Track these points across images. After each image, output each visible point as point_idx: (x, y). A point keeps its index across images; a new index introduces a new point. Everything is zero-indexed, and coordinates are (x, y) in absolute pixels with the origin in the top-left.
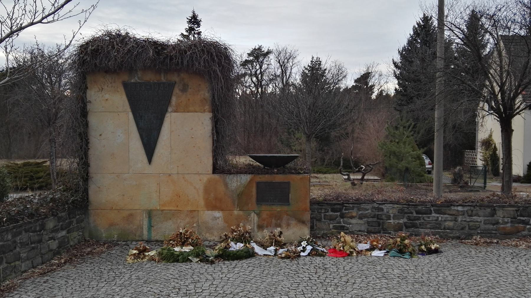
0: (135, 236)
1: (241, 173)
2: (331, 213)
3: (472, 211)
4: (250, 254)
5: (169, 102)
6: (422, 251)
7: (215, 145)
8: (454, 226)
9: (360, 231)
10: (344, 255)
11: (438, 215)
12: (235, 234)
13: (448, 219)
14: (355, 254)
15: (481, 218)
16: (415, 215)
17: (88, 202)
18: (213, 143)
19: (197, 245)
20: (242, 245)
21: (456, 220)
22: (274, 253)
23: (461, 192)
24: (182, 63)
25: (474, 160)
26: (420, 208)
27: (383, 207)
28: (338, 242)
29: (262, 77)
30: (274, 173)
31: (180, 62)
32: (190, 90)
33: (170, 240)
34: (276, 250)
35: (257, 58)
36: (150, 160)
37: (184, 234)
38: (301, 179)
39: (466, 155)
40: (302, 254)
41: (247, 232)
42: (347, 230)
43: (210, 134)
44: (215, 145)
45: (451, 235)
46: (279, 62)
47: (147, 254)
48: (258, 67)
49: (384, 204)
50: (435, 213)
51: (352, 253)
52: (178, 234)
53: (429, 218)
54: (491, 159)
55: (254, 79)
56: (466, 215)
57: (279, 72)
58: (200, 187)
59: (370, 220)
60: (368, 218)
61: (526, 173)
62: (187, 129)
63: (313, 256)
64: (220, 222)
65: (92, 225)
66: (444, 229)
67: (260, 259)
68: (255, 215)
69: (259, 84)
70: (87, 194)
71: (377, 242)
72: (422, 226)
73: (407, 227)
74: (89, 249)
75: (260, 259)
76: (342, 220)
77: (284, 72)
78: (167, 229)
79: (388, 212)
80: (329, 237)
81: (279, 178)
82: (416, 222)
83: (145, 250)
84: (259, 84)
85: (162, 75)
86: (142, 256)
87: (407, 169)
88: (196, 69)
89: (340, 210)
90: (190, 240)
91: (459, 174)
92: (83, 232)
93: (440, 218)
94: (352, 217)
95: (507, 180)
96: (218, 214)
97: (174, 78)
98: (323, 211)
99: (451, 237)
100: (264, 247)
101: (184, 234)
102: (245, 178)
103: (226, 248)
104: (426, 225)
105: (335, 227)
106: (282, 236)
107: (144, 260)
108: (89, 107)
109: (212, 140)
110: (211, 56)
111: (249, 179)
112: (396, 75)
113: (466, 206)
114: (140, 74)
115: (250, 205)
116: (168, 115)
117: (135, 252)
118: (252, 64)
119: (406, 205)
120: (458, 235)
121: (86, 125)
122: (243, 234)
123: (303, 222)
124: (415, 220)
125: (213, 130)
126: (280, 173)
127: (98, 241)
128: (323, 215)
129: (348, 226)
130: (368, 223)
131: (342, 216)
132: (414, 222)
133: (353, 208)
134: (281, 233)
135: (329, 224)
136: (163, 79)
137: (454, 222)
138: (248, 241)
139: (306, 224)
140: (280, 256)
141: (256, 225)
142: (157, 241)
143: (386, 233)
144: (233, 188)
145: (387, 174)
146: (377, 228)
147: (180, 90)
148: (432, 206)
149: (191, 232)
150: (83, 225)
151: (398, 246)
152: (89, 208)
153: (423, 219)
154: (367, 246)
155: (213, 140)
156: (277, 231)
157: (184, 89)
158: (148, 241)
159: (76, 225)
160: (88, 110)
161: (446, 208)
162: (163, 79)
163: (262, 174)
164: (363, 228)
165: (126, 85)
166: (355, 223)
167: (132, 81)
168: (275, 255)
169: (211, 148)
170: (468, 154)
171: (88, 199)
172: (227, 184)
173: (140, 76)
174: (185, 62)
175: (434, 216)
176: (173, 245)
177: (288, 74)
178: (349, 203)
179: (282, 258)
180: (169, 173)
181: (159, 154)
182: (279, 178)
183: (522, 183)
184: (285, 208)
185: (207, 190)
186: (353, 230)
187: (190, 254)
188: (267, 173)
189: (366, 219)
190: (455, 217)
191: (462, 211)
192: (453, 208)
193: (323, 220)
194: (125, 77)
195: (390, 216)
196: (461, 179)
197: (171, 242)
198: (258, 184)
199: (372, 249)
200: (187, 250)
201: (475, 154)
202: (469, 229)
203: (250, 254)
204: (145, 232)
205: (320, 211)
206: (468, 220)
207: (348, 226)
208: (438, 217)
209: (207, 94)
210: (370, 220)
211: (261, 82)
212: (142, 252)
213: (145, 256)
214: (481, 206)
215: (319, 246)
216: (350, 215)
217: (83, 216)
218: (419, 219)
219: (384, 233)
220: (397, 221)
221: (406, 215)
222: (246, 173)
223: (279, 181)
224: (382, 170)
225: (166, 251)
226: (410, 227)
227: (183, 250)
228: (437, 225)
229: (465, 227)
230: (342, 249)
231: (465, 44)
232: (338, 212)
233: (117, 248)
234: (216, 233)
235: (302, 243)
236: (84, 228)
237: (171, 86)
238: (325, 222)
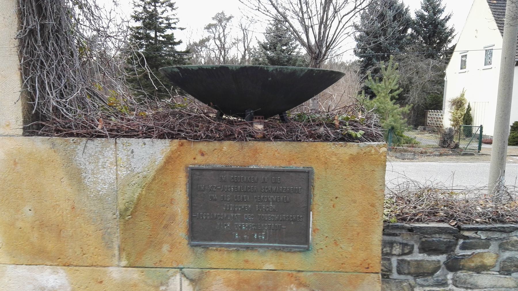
1: (131, 133)
23: (453, 155)
25: (440, 119)
29: (225, 40)
30: (252, 136)
35: (220, 21)
38: (354, 159)
39: (428, 115)
48: (221, 30)
54: (464, 119)
55: (218, 42)
68: (186, 283)
69: (222, 48)
76: (450, 276)
77: (245, 36)
81: (273, 155)
84: (222, 48)
89: (448, 248)
91: (449, 134)
94: (480, 269)
102: (149, 153)
111: (160, 159)
112: (355, 37)
115: (166, 248)
118: (216, 28)
126: (277, 138)
133: (486, 245)
144: (103, 188)
163: (209, 138)
172: (79, 172)
178: (476, 230)
184: (293, 261)
188: (229, 137)
196: (451, 141)
198: (195, 175)
201: (440, 114)
211: (224, 45)
216: (476, 262)
222: (148, 134)
223: (271, 167)
232: (442, 253)
238: (401, 282)
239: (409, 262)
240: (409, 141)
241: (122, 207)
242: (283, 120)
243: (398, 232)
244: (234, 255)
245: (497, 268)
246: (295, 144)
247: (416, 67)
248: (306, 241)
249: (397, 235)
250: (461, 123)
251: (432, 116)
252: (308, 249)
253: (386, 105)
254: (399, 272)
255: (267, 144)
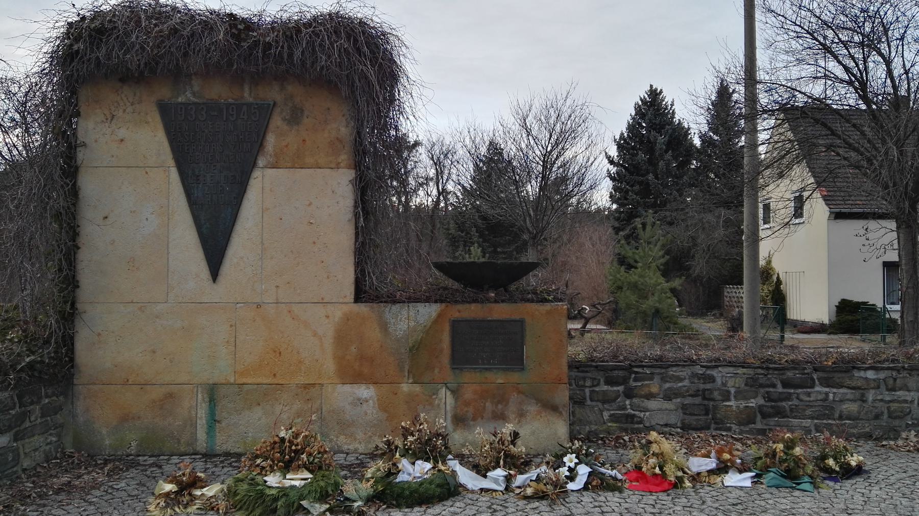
0: (179, 442)
1: (417, 300)
2: (606, 388)
3: (895, 380)
4: (449, 490)
5: (260, 146)
6: (828, 470)
7: (361, 239)
8: (859, 413)
9: (666, 425)
10: (666, 485)
11: (827, 390)
12: (410, 438)
13: (849, 397)
14: (688, 484)
15: (912, 394)
16: (780, 389)
17: (72, 367)
18: (357, 234)
19: (320, 468)
20: (428, 466)
21: (863, 400)
22: (504, 486)
24: (291, 55)
26: (790, 374)
27: (714, 373)
28: (645, 455)
30: (488, 300)
31: (285, 56)
32: (306, 121)
33: (257, 457)
34: (508, 479)
36: (215, 273)
37: (290, 441)
38: (549, 313)
39: (726, 294)
40: (571, 486)
41: (438, 435)
42: (640, 422)
43: (350, 215)
44: (361, 239)
45: (855, 431)
46: (432, 159)
47: (198, 493)
49: (717, 367)
50: (821, 384)
51: (680, 480)
52: (275, 443)
53: (809, 395)
54: (772, 298)
56: (883, 387)
57: (432, 173)
58: (328, 331)
59: (688, 401)
60: (684, 397)
61: (834, 319)
62: (298, 207)
63: (595, 489)
64: (371, 410)
65: (81, 419)
66: (841, 418)
67: (474, 502)
68: (449, 393)
70: (71, 350)
71: (730, 453)
72: (795, 412)
73: (764, 416)
74: (65, 479)
75: (474, 502)
76: (628, 402)
77: (439, 174)
78: (252, 427)
79: (724, 384)
80: (602, 439)
81: (501, 311)
82: (784, 404)
83: (196, 483)
85: (247, 89)
86: (186, 499)
87: (657, 312)
88: (322, 68)
89: (624, 381)
90: (304, 456)
92: (59, 436)
93: (831, 396)
94: (650, 396)
95: (910, 319)
96: (365, 392)
97: (272, 93)
98: (588, 383)
99: (854, 435)
100: (482, 471)
101: (290, 441)
102: (427, 312)
103: (389, 474)
104: (805, 410)
105: (614, 418)
106: (519, 442)
107: (189, 510)
108: (81, 155)
109: (353, 227)
110: (355, 44)
111: (434, 315)
113: (883, 369)
114: (196, 84)
115: (436, 371)
116: (257, 173)
117: (169, 487)
119: (762, 368)
120: (867, 430)
121: (74, 193)
122: (430, 439)
123: (554, 409)
124: (782, 400)
125: (356, 207)
126: (503, 301)
127: (91, 456)
128: (587, 391)
129: (642, 415)
130: (684, 407)
131: (629, 394)
132: (780, 404)
133: (651, 377)
134: (516, 435)
135: (601, 411)
136: (246, 95)
137: (859, 403)
138: (441, 456)
139: (561, 413)
140: (518, 491)
141: (449, 415)
142: (228, 454)
143: (720, 429)
144: (400, 334)
145: (618, 322)
146: (702, 418)
147: (284, 119)
148: (816, 370)
149: (306, 436)
150: (59, 418)
151: (782, 461)
152: (75, 381)
153: (798, 398)
154: (711, 463)
155: (356, 228)
156: (507, 429)
157: (295, 117)
158: (208, 456)
159: (39, 420)
160: (79, 162)
161: (843, 375)
162: (248, 96)
163: (463, 302)
164: (674, 419)
165: (164, 109)
166: (658, 409)
167: (180, 100)
168: (508, 489)
169: (353, 247)
170: (730, 292)
171: (72, 360)
173: (196, 88)
174: (298, 53)
175: (820, 392)
176: (263, 468)
177: (445, 177)
178: (643, 367)
179: (526, 498)
180: (258, 300)
181: (235, 260)
182: (501, 311)
183: (830, 334)
184: (515, 377)
185: (341, 338)
186: (653, 423)
187: (306, 492)
189: (679, 400)
190: (861, 391)
191: (874, 380)
192: (856, 374)
193: (589, 402)
194: (165, 92)
195: (729, 392)
197: (259, 461)
198: (456, 325)
199: (723, 469)
200: (297, 483)
202: (889, 417)
203: (449, 490)
204: (201, 435)
205: (581, 383)
206: (888, 398)
207: (642, 415)
208: (827, 394)
209: (343, 130)
210: (688, 401)
212: (187, 487)
213: (193, 498)
214: (911, 370)
215: (603, 465)
217: (61, 398)
218: (788, 397)
219: (716, 429)
220: (743, 404)
221: (762, 390)
222: (427, 300)
224: (608, 315)
225: (246, 487)
226: (770, 416)
227: (287, 483)
228: (826, 410)
229: (882, 413)
230: (657, 470)
231: (710, 129)
233: (133, 472)
234: (360, 435)
235: (565, 459)
236: (62, 426)
237: (265, 111)
238: (593, 407)
239: (597, 392)
240: (683, 329)
241: (411, 345)
242: (506, 290)
243: (588, 369)
244: (478, 374)
245: (661, 396)
246: (514, 305)
247: (701, 220)
248: (522, 364)
249: (587, 372)
250: (770, 305)
251: (731, 295)
252: (523, 369)
253: (647, 279)
254: (592, 400)
255: (497, 305)
